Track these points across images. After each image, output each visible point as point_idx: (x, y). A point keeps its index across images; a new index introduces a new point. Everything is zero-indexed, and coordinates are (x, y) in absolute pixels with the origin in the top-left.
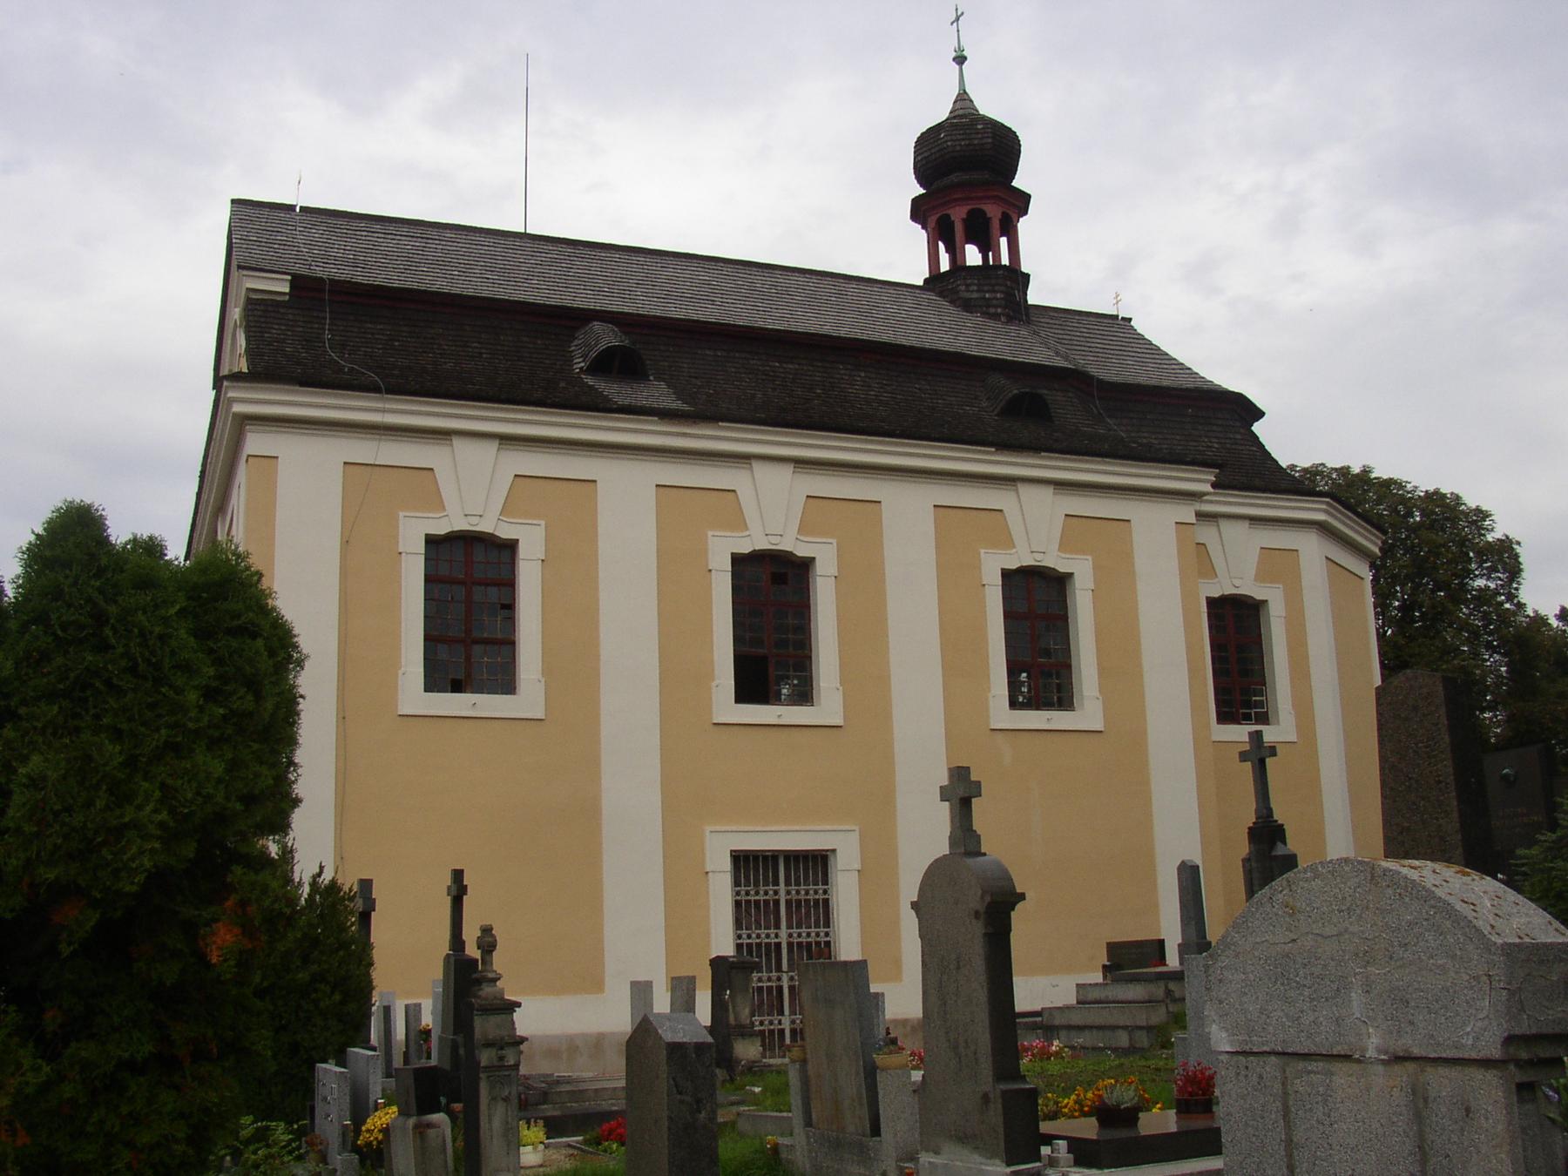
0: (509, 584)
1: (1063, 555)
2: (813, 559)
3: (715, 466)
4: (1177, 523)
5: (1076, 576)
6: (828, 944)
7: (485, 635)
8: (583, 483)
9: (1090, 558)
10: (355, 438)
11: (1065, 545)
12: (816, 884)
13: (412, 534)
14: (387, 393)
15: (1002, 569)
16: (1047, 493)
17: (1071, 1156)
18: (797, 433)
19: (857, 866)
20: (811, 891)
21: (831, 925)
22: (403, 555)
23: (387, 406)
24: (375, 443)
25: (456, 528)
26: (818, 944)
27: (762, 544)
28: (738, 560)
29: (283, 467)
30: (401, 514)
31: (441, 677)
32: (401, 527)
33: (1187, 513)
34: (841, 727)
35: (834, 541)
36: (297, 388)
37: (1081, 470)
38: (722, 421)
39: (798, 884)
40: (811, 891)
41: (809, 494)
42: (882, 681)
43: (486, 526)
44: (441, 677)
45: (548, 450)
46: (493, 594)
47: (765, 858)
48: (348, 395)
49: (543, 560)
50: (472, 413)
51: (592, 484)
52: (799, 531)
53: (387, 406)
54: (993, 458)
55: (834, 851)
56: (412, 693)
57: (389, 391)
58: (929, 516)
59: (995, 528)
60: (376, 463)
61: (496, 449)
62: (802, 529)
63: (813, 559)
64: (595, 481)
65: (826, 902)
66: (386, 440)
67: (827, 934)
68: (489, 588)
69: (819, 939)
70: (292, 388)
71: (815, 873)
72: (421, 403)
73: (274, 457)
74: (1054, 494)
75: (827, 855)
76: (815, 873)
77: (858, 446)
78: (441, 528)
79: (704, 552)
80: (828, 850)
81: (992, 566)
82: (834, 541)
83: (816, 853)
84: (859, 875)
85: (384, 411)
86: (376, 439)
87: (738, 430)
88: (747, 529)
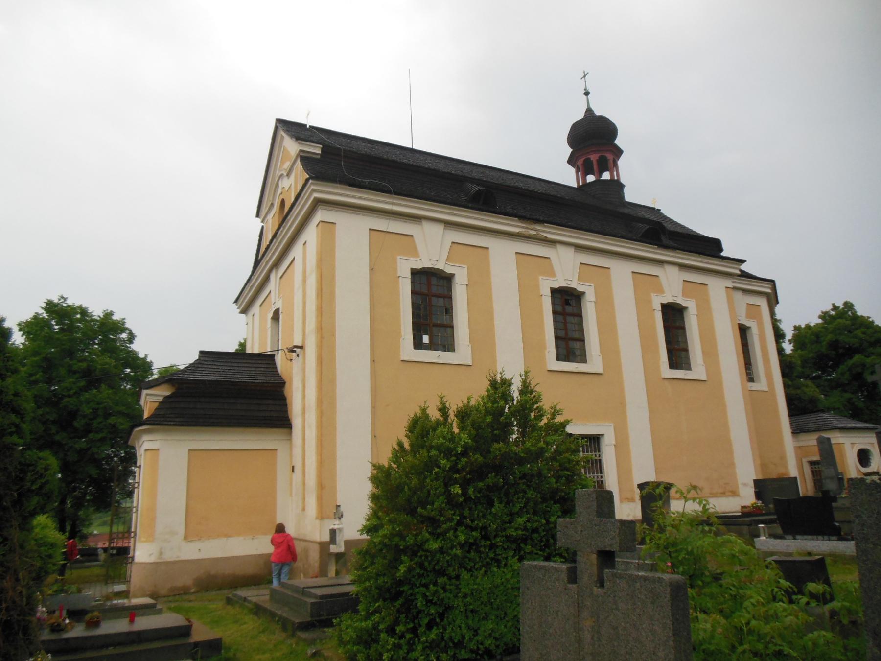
0: (448, 297)
1: (684, 298)
2: (454, 274)
3: (691, 272)
4: (684, 280)
5: (456, 275)
6: (602, 482)
7: (439, 322)
8: (380, 232)
9: (694, 300)
10: (454, 230)
11: (685, 294)
12: (595, 452)
13: (404, 267)
14: (394, 194)
15: (661, 303)
16: (439, 229)
17: (400, 598)
18: (436, 205)
19: (614, 442)
20: (592, 455)
21: (603, 472)
22: (400, 278)
23: (395, 201)
24: (388, 221)
25: (561, 286)
26: (598, 482)
27: (563, 284)
28: (415, 273)
29: (612, 271)
30: (399, 257)
31: (673, 365)
32: (399, 264)
33: (729, 283)
34: (601, 374)
35: (466, 266)
36: (348, 187)
37: (486, 221)
38: (546, 223)
39: (587, 452)
40: (592, 455)
41: (454, 241)
42: (617, 352)
43: (440, 266)
44: (673, 365)
45: (458, 229)
46: (441, 301)
47: (594, 438)
48: (354, 189)
49: (467, 285)
50: (350, 194)
51: (485, 250)
52: (578, 280)
53: (395, 201)
54: (656, 251)
55: (602, 435)
56: (407, 350)
57: (395, 194)
58: (629, 277)
59: (407, 243)
60: (388, 231)
61: (443, 229)
62: (580, 278)
63: (454, 274)
64: (488, 248)
65: (600, 460)
66: (393, 220)
67: (601, 477)
68: (439, 299)
69: (598, 480)
70: (344, 186)
71: (595, 448)
72: (485, 215)
73: (705, 284)
74: (575, 251)
75: (599, 437)
76: (595, 448)
77: (636, 247)
78: (419, 266)
79: (537, 286)
80: (599, 435)
81: (546, 287)
82: (466, 266)
83: (594, 436)
84: (615, 447)
85: (392, 204)
86: (387, 219)
87: (623, 242)
88: (419, 257)
